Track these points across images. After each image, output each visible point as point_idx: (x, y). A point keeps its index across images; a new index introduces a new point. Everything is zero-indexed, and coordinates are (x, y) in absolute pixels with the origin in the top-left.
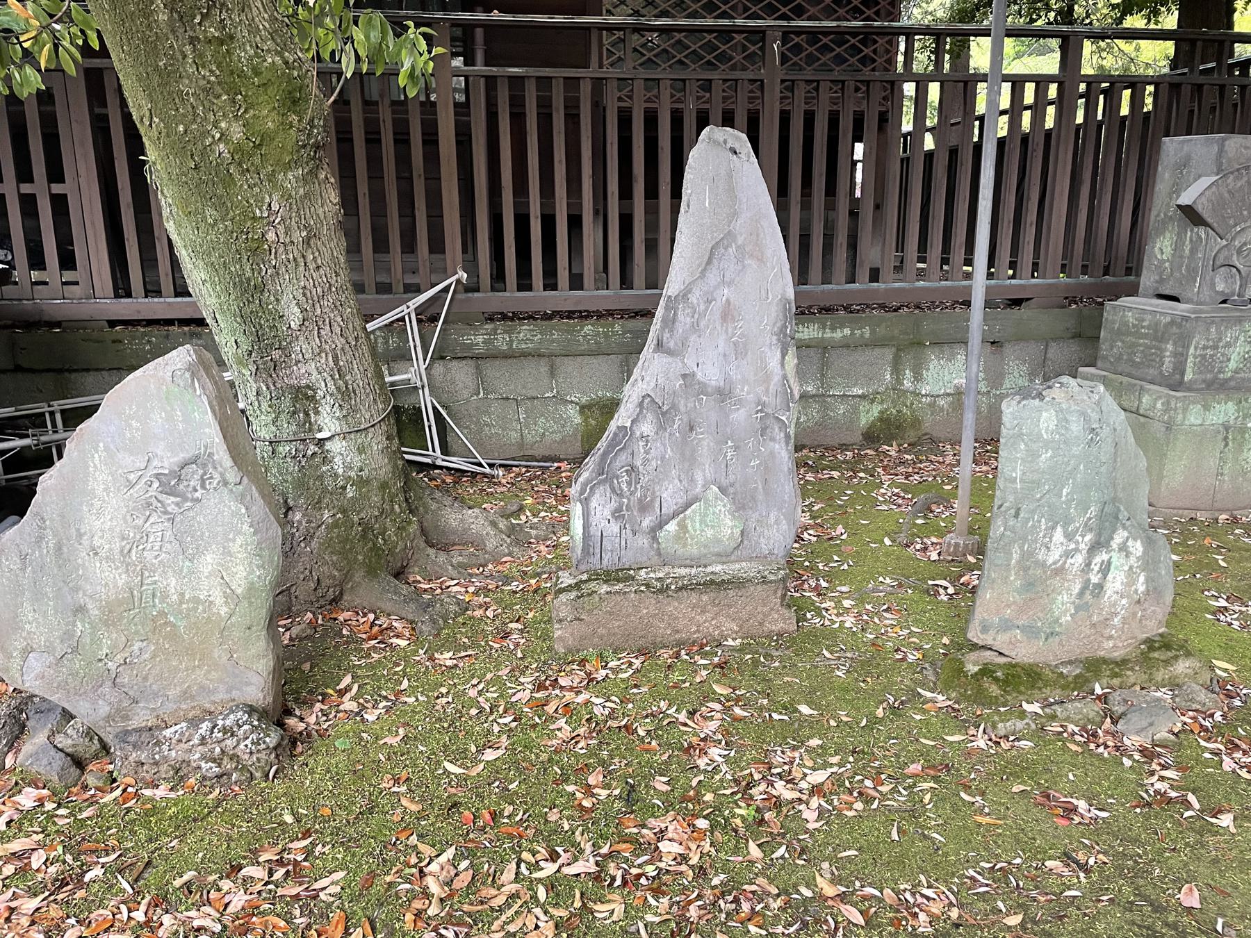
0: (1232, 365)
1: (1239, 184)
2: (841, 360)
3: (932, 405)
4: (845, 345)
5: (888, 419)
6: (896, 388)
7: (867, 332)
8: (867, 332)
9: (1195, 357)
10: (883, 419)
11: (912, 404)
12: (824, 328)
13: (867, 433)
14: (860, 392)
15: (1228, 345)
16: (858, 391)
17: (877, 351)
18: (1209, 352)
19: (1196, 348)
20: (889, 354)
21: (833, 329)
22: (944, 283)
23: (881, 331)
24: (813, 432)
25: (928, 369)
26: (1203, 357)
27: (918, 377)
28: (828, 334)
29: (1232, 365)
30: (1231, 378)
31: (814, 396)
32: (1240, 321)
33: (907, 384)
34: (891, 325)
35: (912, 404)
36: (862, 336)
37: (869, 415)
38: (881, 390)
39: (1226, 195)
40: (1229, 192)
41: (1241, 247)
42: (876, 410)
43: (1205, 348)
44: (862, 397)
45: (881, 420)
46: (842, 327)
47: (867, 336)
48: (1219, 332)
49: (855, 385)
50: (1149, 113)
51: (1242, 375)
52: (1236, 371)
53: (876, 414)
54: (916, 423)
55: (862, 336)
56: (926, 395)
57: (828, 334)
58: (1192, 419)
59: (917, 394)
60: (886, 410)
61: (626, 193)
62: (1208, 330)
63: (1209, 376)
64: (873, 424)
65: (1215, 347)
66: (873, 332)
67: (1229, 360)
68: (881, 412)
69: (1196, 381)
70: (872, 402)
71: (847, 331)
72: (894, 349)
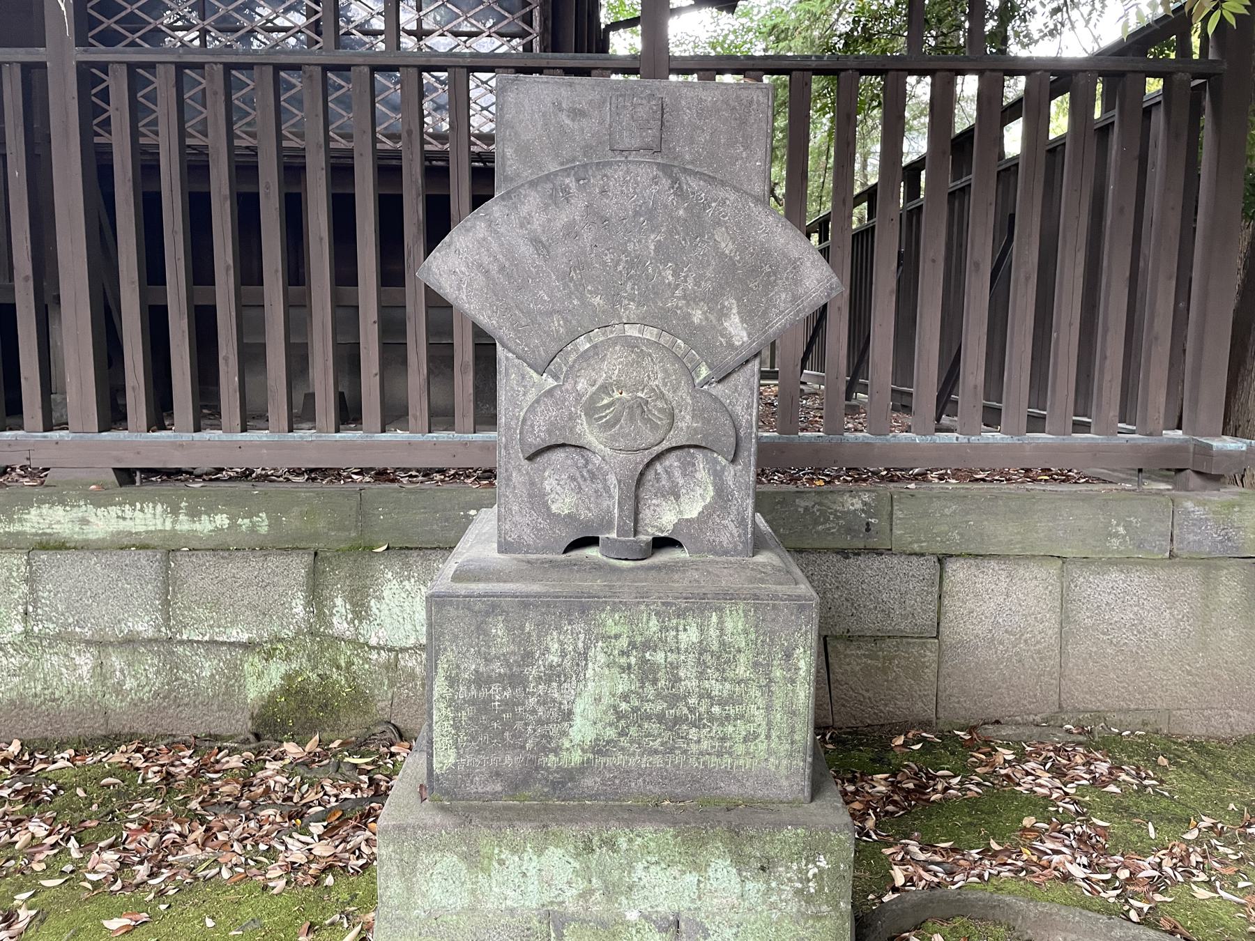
0: (582, 730)
1: (563, 218)
2: (199, 577)
3: (392, 667)
4: (219, 548)
5: (302, 690)
6: (317, 634)
7: (263, 523)
8: (263, 523)
9: (451, 702)
10: (292, 690)
11: (350, 664)
12: (175, 511)
13: (260, 715)
14: (244, 637)
15: (554, 675)
16: (239, 634)
17: (274, 562)
18: (497, 693)
19: (452, 681)
20: (298, 566)
21: (194, 514)
22: (441, 436)
23: (291, 521)
24: (151, 710)
25: (380, 599)
26: (483, 706)
27: (360, 611)
28: (184, 524)
29: (582, 730)
30: (583, 769)
31: (150, 640)
32: (584, 610)
33: (340, 624)
34: (308, 510)
35: (350, 664)
36: (253, 529)
37: (262, 681)
38: (287, 633)
39: (525, 250)
40: (535, 241)
41: (593, 399)
42: (276, 673)
43: (481, 680)
44: (248, 646)
45: (286, 692)
46: (211, 510)
47: (264, 529)
48: (520, 638)
49: (233, 623)
50: (969, 132)
51: (620, 759)
52: (599, 748)
53: (277, 681)
54: (360, 700)
55: (253, 529)
56: (379, 648)
57: (184, 524)
58: (436, 893)
59: (359, 645)
60: (298, 673)
61: (345, 273)
62: (481, 629)
63: (510, 761)
64: (272, 699)
65: (515, 680)
66: (274, 523)
67: (568, 716)
68: (288, 677)
69: (469, 774)
70: (269, 656)
71: (222, 520)
72: (308, 559)
